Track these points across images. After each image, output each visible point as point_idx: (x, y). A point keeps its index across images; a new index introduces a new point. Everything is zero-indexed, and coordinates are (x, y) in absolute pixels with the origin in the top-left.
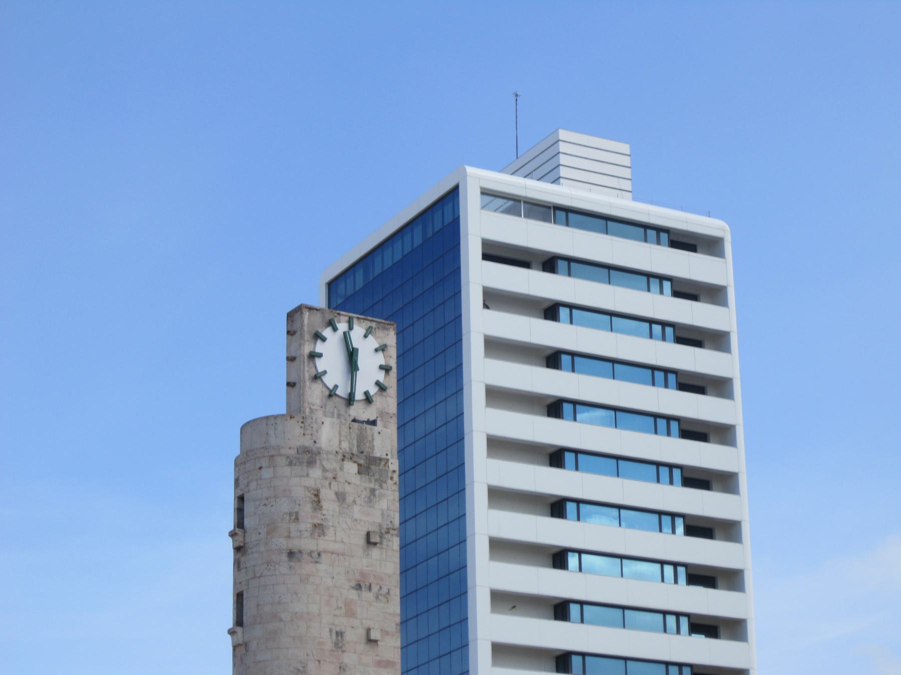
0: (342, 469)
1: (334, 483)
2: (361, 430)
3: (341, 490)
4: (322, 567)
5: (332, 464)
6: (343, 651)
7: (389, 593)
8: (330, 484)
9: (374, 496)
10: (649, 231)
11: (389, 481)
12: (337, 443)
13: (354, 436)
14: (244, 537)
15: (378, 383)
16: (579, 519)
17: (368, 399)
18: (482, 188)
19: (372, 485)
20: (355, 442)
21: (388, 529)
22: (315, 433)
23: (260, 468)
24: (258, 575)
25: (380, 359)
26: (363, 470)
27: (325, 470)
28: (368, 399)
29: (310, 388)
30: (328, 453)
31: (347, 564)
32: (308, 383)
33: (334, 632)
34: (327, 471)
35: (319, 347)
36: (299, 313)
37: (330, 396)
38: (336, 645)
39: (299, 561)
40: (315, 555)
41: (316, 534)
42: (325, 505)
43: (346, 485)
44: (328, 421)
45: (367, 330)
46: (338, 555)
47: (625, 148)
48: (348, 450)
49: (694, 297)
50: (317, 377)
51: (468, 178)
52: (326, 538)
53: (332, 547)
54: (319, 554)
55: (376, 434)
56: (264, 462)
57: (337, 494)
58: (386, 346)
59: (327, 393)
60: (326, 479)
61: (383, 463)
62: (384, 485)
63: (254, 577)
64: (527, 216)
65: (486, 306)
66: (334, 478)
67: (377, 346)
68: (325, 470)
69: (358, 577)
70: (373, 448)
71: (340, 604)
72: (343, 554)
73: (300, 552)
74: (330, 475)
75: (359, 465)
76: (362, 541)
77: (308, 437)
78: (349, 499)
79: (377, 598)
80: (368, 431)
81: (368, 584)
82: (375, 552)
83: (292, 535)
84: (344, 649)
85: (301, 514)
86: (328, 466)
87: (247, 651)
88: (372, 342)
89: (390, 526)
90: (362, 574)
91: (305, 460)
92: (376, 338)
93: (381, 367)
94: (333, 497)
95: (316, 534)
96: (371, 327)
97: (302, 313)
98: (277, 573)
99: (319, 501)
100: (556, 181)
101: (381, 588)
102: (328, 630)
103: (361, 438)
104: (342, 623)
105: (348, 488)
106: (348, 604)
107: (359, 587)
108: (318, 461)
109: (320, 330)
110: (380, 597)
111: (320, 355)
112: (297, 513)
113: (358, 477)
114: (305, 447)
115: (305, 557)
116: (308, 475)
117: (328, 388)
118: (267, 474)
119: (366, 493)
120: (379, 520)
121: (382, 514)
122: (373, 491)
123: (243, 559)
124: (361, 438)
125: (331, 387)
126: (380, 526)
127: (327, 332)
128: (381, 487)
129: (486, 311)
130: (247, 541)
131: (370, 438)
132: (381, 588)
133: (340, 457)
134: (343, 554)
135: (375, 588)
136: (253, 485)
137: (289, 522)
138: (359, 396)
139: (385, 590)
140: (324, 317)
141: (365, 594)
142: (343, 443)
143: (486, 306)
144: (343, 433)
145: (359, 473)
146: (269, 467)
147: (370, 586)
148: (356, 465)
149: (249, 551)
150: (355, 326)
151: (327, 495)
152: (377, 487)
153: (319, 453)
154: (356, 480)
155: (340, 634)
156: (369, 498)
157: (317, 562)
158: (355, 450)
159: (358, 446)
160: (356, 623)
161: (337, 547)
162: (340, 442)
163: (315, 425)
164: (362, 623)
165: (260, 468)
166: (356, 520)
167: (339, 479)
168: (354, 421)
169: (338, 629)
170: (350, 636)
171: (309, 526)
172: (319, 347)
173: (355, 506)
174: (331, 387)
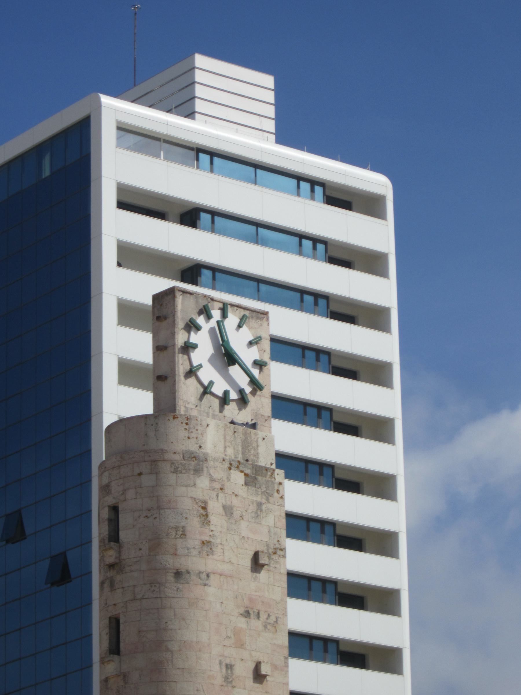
0: (229, 479)
1: (221, 495)
2: (245, 434)
3: (229, 503)
4: (211, 590)
5: (219, 472)
6: (234, 687)
7: (276, 622)
8: (217, 496)
9: (261, 510)
10: (302, 183)
11: (276, 494)
12: (222, 450)
13: (239, 441)
14: (120, 552)
18: (118, 122)
19: (259, 499)
20: (240, 448)
21: (275, 549)
22: (199, 436)
23: (140, 474)
24: (139, 597)
26: (250, 481)
27: (212, 480)
30: (215, 460)
31: (236, 587)
33: (224, 664)
34: (214, 481)
35: (194, 338)
36: (170, 297)
38: (226, 678)
39: (188, 583)
40: (204, 576)
41: (204, 552)
42: (212, 518)
43: (234, 497)
44: (212, 423)
45: (241, 320)
46: (227, 576)
47: (269, 81)
48: (233, 457)
49: (347, 264)
50: (192, 372)
51: (103, 110)
52: (215, 557)
54: (208, 576)
55: (260, 440)
56: (145, 468)
57: (224, 507)
60: (214, 489)
61: (269, 474)
62: (271, 499)
63: (134, 599)
64: (166, 158)
65: (119, 265)
66: (221, 489)
67: (251, 338)
68: (212, 480)
69: (247, 602)
70: (257, 455)
71: (230, 634)
72: (231, 577)
73: (188, 572)
74: (218, 486)
75: (246, 475)
76: (248, 563)
77: (193, 441)
78: (237, 514)
79: (265, 627)
80: (253, 436)
81: (256, 611)
82: (263, 574)
83: (179, 553)
84: (234, 684)
85: (188, 528)
86: (215, 476)
87: (126, 683)
89: (277, 546)
90: (251, 600)
91: (192, 468)
92: (250, 328)
94: (221, 511)
95: (204, 552)
96: (244, 316)
97: (174, 297)
99: (207, 515)
100: (191, 115)
101: (269, 616)
102: (217, 661)
103: (246, 445)
104: (232, 654)
105: (235, 502)
106: (237, 632)
107: (247, 614)
108: (205, 469)
109: (194, 317)
110: (269, 627)
111: (194, 347)
112: (184, 527)
113: (245, 488)
114: (191, 453)
115: (193, 577)
116: (195, 484)
117: (201, 384)
118: (147, 481)
119: (253, 508)
120: (266, 539)
121: (269, 532)
122: (259, 505)
123: (118, 578)
124: (246, 445)
125: (206, 383)
126: (267, 545)
127: (201, 320)
128: (267, 500)
129: (121, 270)
130: (123, 557)
131: (254, 445)
132: (269, 616)
133: (227, 465)
134: (231, 577)
135: (263, 616)
136: (131, 494)
137: (176, 538)
139: (272, 619)
140: (197, 302)
142: (228, 449)
143: (119, 265)
144: (228, 438)
145: (246, 484)
146: (150, 473)
147: (258, 613)
148: (243, 474)
149: (127, 569)
151: (215, 507)
152: (264, 501)
153: (206, 460)
154: (243, 491)
155: (229, 667)
156: (256, 513)
157: (205, 585)
158: (240, 458)
159: (243, 454)
160: (245, 654)
162: (225, 447)
163: (199, 428)
164: (251, 655)
165: (140, 474)
166: (243, 537)
167: (226, 490)
168: (232, 422)
169: (228, 661)
171: (197, 543)
172: (194, 338)
173: (242, 521)
174: (206, 383)
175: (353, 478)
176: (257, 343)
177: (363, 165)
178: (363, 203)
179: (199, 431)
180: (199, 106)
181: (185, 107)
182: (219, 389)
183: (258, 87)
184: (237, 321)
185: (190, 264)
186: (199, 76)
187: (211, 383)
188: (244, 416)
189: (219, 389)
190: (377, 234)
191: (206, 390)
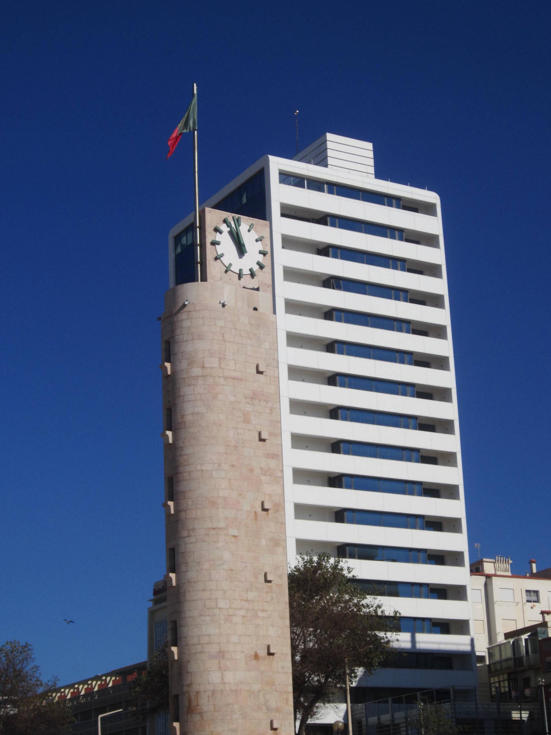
15: (258, 263)
17: (252, 274)
18: (280, 170)
25: (259, 246)
28: (252, 274)
32: (211, 262)
37: (226, 272)
45: (250, 226)
47: (370, 146)
58: (263, 237)
59: (225, 268)
65: (283, 247)
67: (257, 237)
88: (254, 235)
93: (260, 252)
98: (196, 393)
100: (326, 166)
125: (227, 266)
129: (283, 250)
143: (283, 247)
150: (242, 224)
175: (426, 360)
176: (261, 240)
177: (422, 187)
178: (426, 208)
179: (260, 309)
180: (330, 161)
181: (322, 161)
182: (235, 268)
183: (364, 151)
184: (248, 228)
185: (324, 246)
186: (329, 145)
187: (230, 265)
188: (254, 283)
189: (235, 268)
190: (433, 225)
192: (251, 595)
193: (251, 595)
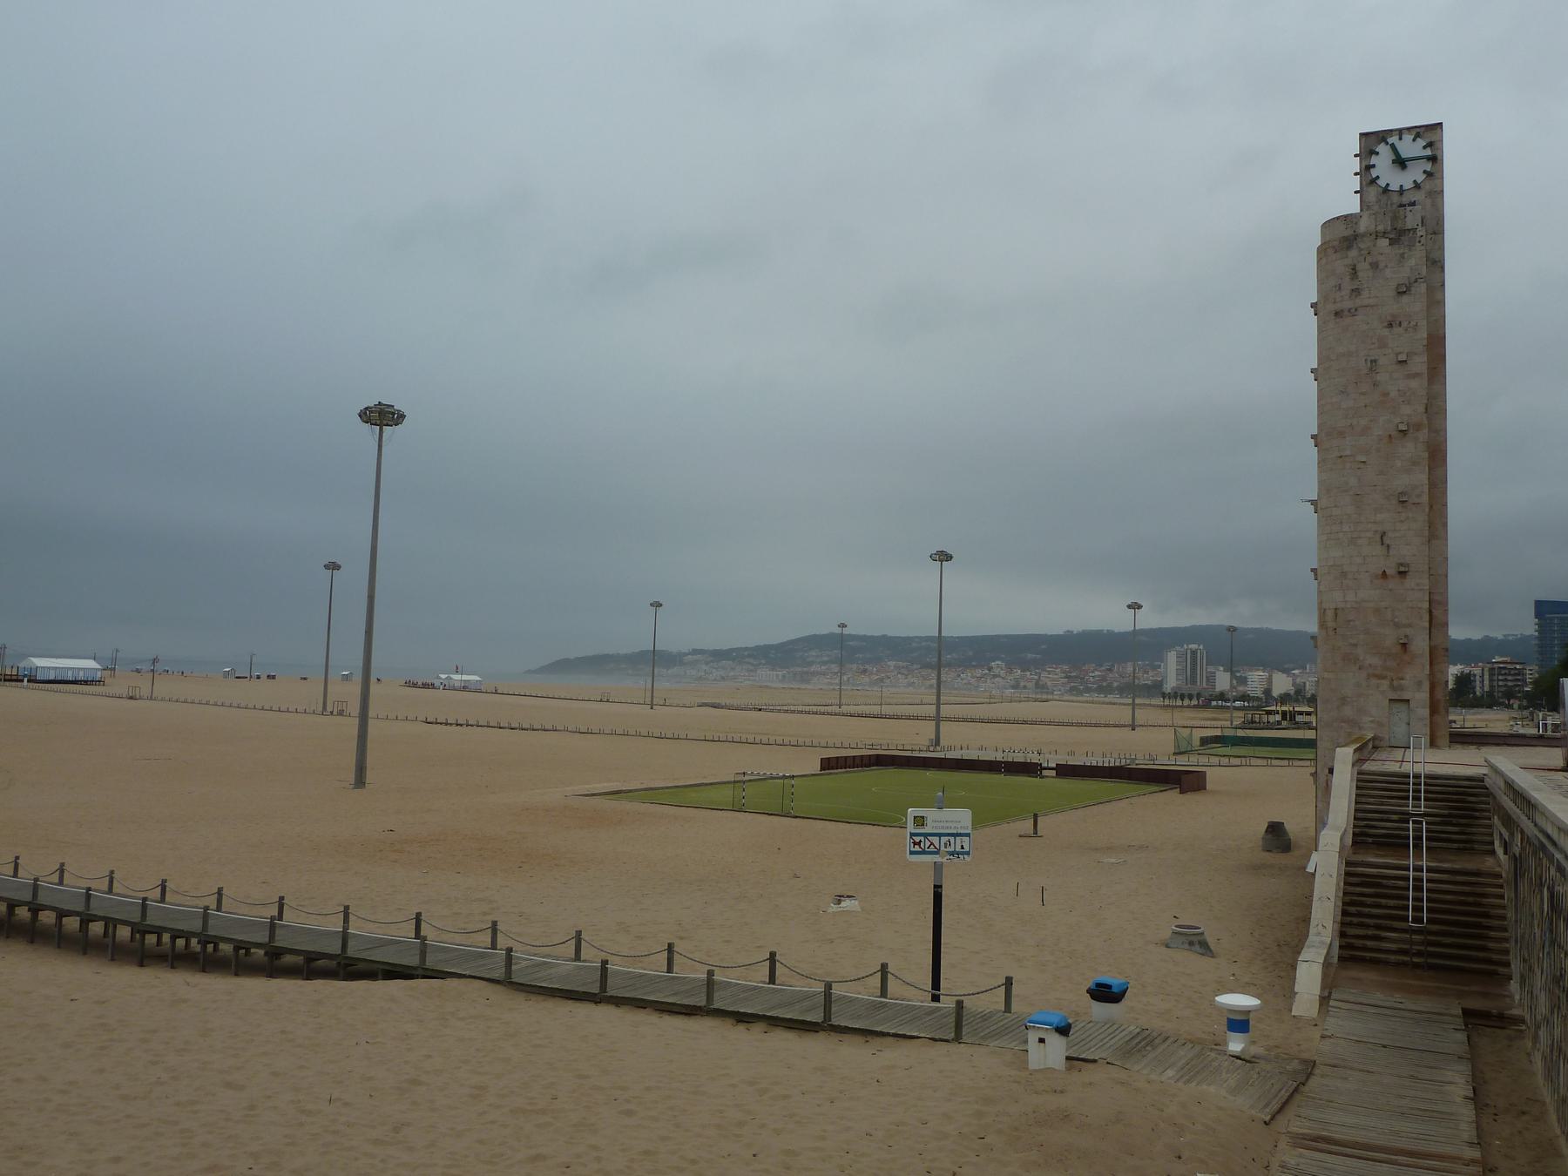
16: (1068, 1058)
29: (950, 748)
42: (1360, 274)
53: (1366, 302)
78: (1382, 265)
82: (1405, 299)
103: (1395, 218)
105: (1381, 258)
107: (1390, 325)
135: (1405, 324)
138: (1428, 152)
141: (1396, 330)
151: (1363, 267)
161: (1371, 301)
170: (1382, 361)
191: (1417, 186)
192: (1379, 517)
193: (1379, 517)
